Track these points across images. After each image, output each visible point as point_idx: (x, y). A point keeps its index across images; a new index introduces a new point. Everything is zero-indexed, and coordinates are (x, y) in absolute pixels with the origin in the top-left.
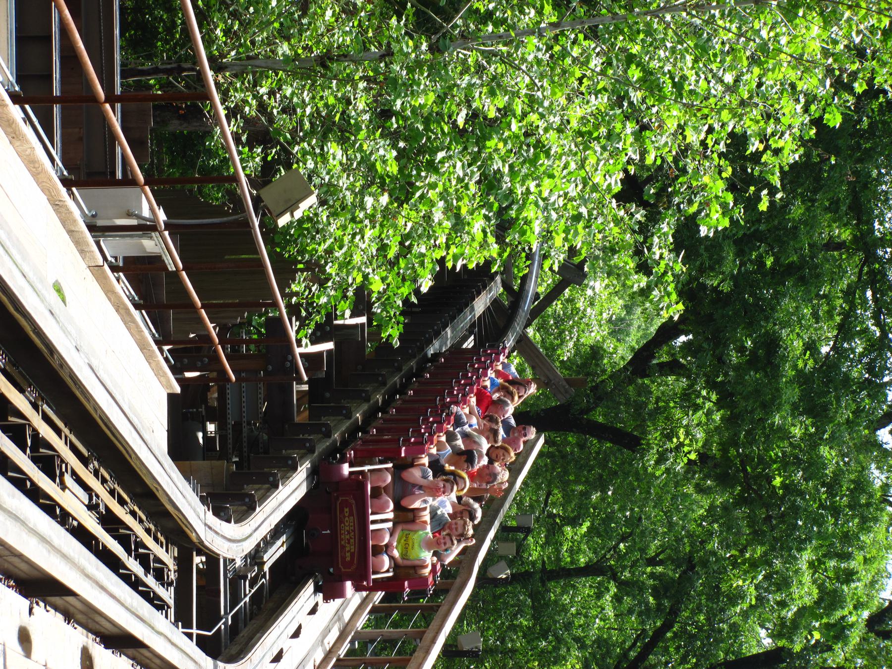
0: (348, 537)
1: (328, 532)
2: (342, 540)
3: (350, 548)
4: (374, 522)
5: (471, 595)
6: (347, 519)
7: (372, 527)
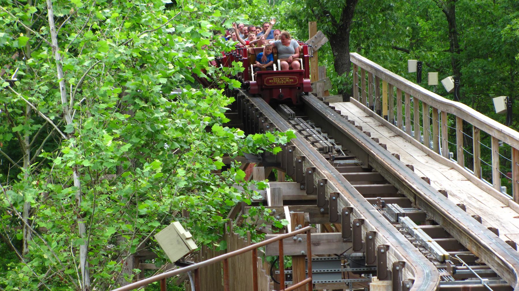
0: (282, 81)
1: (280, 90)
2: (284, 83)
3: (287, 80)
4: (277, 69)
5: (465, 103)
6: (274, 81)
7: (280, 69)
